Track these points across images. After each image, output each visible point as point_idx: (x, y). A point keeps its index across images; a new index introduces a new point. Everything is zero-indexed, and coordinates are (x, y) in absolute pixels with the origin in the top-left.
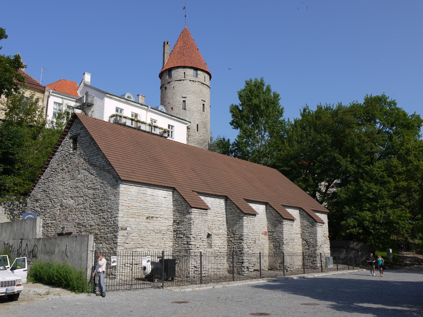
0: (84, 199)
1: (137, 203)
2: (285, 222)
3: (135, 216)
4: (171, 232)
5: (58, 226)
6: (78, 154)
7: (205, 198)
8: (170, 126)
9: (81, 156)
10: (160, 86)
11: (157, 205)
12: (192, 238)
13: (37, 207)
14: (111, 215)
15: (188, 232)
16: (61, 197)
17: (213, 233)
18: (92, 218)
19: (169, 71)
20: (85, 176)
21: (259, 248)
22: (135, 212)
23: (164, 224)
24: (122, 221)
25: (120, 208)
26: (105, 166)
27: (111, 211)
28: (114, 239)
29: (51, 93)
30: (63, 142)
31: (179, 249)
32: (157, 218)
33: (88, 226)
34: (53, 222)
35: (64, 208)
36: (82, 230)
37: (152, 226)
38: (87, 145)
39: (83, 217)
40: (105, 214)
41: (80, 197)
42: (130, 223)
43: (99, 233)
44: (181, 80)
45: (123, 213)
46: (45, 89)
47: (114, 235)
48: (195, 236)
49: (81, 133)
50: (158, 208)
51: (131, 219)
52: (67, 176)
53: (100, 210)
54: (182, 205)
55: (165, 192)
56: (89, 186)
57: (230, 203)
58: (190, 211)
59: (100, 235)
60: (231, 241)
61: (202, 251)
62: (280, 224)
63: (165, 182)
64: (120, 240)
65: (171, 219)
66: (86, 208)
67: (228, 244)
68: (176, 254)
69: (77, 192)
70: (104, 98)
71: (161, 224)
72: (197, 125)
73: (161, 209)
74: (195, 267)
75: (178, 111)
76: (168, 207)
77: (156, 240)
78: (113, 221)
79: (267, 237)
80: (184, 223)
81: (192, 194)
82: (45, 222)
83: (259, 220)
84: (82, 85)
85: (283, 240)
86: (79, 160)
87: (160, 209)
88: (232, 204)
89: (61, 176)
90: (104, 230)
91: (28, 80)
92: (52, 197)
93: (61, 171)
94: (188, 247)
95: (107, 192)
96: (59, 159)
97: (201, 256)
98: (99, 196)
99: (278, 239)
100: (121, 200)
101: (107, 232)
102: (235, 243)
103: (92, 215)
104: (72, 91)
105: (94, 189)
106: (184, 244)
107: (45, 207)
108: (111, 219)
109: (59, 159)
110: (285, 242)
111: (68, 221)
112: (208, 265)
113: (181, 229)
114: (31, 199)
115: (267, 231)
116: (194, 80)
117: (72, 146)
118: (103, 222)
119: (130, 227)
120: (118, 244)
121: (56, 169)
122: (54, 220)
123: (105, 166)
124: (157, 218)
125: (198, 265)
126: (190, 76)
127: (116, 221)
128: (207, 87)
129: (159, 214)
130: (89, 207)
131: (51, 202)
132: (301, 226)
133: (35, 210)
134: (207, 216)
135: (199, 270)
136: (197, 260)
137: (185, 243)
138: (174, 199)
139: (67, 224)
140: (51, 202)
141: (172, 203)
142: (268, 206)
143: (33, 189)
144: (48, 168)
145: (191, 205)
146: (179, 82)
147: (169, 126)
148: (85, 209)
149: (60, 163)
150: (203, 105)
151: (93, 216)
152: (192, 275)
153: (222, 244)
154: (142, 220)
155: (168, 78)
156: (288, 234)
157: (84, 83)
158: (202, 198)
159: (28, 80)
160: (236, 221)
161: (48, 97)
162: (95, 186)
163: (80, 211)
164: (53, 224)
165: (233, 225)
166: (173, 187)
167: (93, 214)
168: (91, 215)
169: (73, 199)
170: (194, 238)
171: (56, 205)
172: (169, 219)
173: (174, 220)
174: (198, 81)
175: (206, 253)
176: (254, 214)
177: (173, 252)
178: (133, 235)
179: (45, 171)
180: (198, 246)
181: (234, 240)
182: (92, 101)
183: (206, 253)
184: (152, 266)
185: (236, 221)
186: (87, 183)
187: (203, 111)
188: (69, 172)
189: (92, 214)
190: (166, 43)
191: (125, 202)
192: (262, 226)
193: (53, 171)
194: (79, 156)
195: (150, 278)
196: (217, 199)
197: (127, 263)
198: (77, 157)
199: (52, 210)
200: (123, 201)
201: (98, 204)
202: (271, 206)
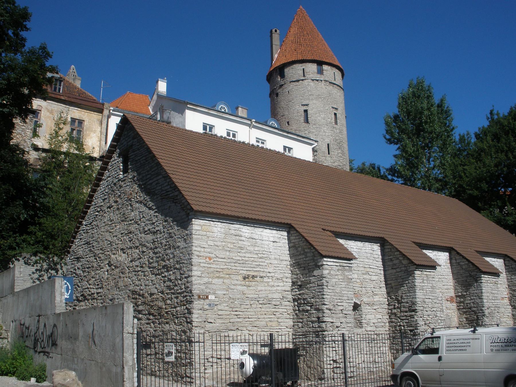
0: (139, 251)
1: (224, 253)
2: (485, 278)
3: (223, 275)
4: (289, 301)
5: (106, 297)
6: (130, 179)
7: (347, 243)
8: (287, 149)
9: (134, 181)
10: (269, 92)
11: (262, 255)
12: (326, 311)
13: (78, 268)
14: (181, 274)
15: (318, 300)
16: (108, 251)
17: (362, 302)
18: (152, 281)
19: (281, 70)
20: (140, 212)
21: (442, 324)
22: (222, 267)
23: (275, 288)
24: (200, 284)
25: (195, 260)
26: (168, 192)
27: (181, 267)
28: (187, 315)
29: (111, 111)
30: (110, 164)
31: (304, 330)
32: (261, 277)
33: (146, 295)
34: (99, 290)
35: (113, 268)
36: (139, 302)
37: (253, 292)
38: (142, 162)
39: (140, 281)
40: (171, 272)
41: (134, 248)
42: (214, 287)
43: (164, 307)
44: (299, 81)
45: (201, 269)
46: (103, 106)
47: (186, 308)
48: (332, 307)
49: (134, 143)
50: (263, 260)
51: (215, 281)
52: (115, 216)
53: (164, 267)
54: (305, 253)
55: (274, 232)
56: (146, 229)
57: (389, 250)
58: (320, 264)
59: (166, 309)
60: (395, 314)
61: (346, 333)
62: (477, 281)
63: (273, 215)
64: (196, 317)
65: (287, 280)
66: (144, 265)
67: (389, 320)
68: (301, 340)
69: (130, 241)
70: (185, 110)
71: (270, 288)
72: (328, 145)
73: (269, 262)
74: (335, 361)
75: (296, 126)
76: (281, 258)
77: (262, 317)
78: (185, 284)
79: (454, 306)
80: (311, 285)
81: (322, 233)
82: (89, 291)
83: (439, 277)
84: (155, 97)
85: (483, 308)
86: (132, 188)
87: (267, 262)
88: (393, 250)
89: (108, 217)
90: (171, 301)
91: (81, 95)
92: (97, 252)
93: (109, 209)
94: (319, 327)
95: (173, 235)
96: (105, 190)
97: (344, 341)
98: (161, 243)
99: (474, 307)
100: (196, 247)
101: (176, 304)
102: (402, 318)
103: (153, 276)
104: (142, 107)
105: (154, 233)
106: (313, 322)
107: (89, 267)
108: (181, 280)
109: (105, 190)
110: (486, 312)
111: (119, 288)
112: (357, 356)
113: (306, 296)
114: (71, 257)
115: (453, 295)
116: (318, 79)
117: (121, 167)
118: (168, 287)
119: (214, 294)
120: (193, 324)
121: (102, 208)
122: (100, 288)
123: (168, 192)
124: (261, 277)
125: (339, 358)
126: (312, 73)
127: (188, 285)
128: (339, 88)
129: (265, 270)
130: (147, 263)
131: (96, 260)
132: (509, 286)
133: (76, 275)
134: (351, 271)
135: (342, 365)
136: (337, 349)
137: (314, 319)
138: (292, 245)
139: (118, 293)
140: (95, 260)
141: (288, 252)
142: (453, 253)
143: (72, 242)
144: (92, 207)
145: (320, 252)
146: (297, 83)
147: (285, 148)
148: (142, 267)
149: (106, 197)
150: (335, 114)
151: (153, 277)
152: (329, 375)
153: (380, 320)
154: (236, 282)
155: (279, 80)
156: (491, 298)
157: (157, 94)
158: (341, 241)
159: (81, 95)
160: (402, 280)
161: (109, 117)
162: (155, 228)
163: (136, 271)
164: (99, 295)
165: (397, 287)
166: (287, 224)
167: (153, 274)
168: (150, 276)
169: (124, 253)
170: (330, 310)
171: (102, 264)
172: (285, 279)
173: (292, 282)
174: (325, 81)
175: (353, 335)
176: (433, 266)
177: (294, 337)
178: (219, 307)
179: (87, 212)
180: (339, 324)
181: (401, 312)
182: (168, 118)
183: (353, 335)
184: (256, 362)
185: (402, 280)
186: (143, 224)
187: (336, 123)
188: (118, 209)
189: (152, 274)
190: (274, 31)
191: (203, 250)
192: (446, 287)
193: (98, 212)
194: (131, 182)
195: (252, 382)
196: (367, 244)
197: (212, 357)
198: (128, 184)
199: (98, 272)
200: (199, 249)
201: (160, 257)
202: (458, 253)
